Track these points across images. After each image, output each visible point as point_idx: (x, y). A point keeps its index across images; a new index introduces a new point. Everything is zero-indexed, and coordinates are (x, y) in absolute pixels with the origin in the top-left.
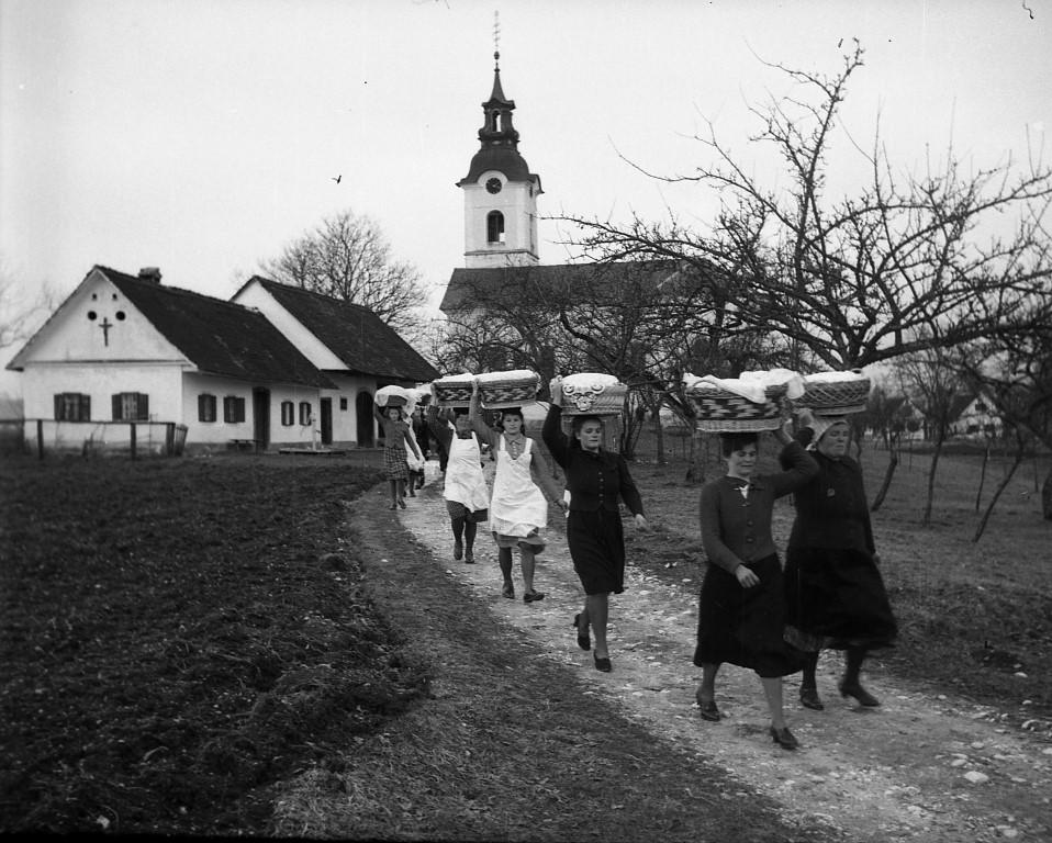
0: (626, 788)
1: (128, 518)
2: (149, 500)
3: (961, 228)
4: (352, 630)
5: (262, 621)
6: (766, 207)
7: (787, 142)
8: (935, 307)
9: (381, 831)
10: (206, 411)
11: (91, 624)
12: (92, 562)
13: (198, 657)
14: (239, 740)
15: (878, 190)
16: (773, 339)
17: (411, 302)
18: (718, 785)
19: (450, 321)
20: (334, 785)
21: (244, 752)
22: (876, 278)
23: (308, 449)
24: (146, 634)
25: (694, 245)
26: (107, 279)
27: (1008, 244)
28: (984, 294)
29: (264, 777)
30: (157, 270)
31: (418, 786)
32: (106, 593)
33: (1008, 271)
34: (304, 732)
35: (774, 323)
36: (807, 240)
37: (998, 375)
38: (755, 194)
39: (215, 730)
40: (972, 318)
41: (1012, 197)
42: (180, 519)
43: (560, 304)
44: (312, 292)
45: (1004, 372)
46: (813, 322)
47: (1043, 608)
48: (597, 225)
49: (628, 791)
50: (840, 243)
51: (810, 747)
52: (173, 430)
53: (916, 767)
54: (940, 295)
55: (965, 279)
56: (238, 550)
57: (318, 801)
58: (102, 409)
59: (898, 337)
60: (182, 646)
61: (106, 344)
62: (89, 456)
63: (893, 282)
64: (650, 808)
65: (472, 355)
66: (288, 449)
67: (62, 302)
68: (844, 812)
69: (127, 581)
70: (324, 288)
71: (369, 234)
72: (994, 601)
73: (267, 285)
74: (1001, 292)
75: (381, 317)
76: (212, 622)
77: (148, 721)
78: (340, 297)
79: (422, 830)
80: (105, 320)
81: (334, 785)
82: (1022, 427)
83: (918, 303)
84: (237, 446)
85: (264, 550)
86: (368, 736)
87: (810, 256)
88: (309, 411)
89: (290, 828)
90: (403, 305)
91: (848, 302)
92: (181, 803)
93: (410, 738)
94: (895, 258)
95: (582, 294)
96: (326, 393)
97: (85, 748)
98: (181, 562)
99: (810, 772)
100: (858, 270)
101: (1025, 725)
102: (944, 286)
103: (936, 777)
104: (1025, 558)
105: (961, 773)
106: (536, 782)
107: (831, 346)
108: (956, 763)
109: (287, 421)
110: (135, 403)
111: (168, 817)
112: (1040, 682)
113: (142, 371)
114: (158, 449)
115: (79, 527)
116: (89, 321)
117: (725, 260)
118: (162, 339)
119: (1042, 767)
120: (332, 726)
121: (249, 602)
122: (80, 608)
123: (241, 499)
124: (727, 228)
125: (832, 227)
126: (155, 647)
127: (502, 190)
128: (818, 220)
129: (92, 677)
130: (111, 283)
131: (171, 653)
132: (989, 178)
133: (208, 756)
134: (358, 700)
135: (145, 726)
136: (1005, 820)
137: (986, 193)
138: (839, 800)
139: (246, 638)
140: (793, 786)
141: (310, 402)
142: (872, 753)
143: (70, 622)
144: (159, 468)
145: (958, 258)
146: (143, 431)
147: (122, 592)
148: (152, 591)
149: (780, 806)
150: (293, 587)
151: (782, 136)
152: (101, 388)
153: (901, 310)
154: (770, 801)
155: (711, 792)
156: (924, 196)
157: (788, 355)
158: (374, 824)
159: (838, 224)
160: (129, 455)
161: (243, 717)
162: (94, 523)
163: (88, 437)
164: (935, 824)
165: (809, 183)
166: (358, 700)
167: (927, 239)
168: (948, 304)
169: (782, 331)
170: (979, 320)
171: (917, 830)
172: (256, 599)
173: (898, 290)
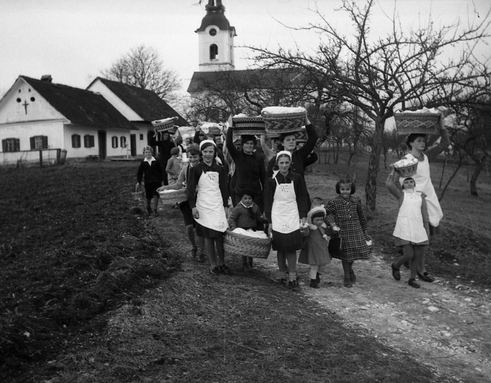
0: (272, 310)
1: (39, 195)
2: (49, 186)
3: (435, 54)
4: (145, 241)
5: (102, 239)
6: (342, 42)
7: (352, 11)
8: (421, 91)
9: (158, 331)
10: (76, 142)
11: (21, 245)
12: (21, 216)
13: (71, 256)
14: (91, 293)
15: (395, 35)
16: (345, 106)
17: (174, 88)
18: (314, 309)
19: (192, 97)
20: (136, 311)
21: (93, 298)
22: (393, 76)
23: (125, 159)
24: (48, 248)
25: (307, 60)
26: (25, 82)
27: (456, 62)
28: (444, 85)
29: (102, 310)
30: (50, 76)
31: (175, 311)
32: (28, 230)
33: (456, 75)
34: (122, 288)
35: (345, 97)
36: (361, 58)
37: (451, 125)
38: (336, 36)
39: (80, 289)
40: (438, 97)
41: (459, 40)
42: (64, 194)
43: (245, 88)
44: (126, 84)
45: (454, 124)
46: (363, 97)
47: (468, 235)
48: (261, 50)
49: (273, 312)
50: (376, 60)
51: (358, 293)
52: (60, 152)
53: (406, 303)
54: (423, 85)
55: (436, 78)
56: (91, 206)
57: (128, 319)
58: (25, 145)
59: (403, 105)
60: (64, 252)
61: (26, 113)
62: (20, 168)
63: (401, 78)
64: (283, 319)
65: (203, 113)
66: (115, 159)
67: (4, 94)
68: (372, 322)
69: (39, 224)
70: (131, 82)
71: (153, 55)
72: (445, 230)
73: (104, 81)
74: (453, 85)
75: (159, 96)
76: (79, 240)
77: (47, 287)
78: (139, 86)
79: (177, 330)
80: (25, 102)
81: (136, 311)
82: (462, 151)
83: (413, 89)
84: (91, 158)
85: (103, 206)
86: (152, 289)
87: (363, 66)
88: (125, 141)
89: (115, 331)
90: (169, 90)
91: (380, 88)
92: (64, 323)
93: (171, 289)
94: (402, 67)
95: (255, 84)
96: (133, 132)
97: (18, 302)
98: (64, 214)
99: (357, 304)
100: (384, 73)
101: (457, 287)
102: (426, 80)
103: (415, 308)
104: (461, 211)
105: (426, 307)
106: (230, 308)
107: (371, 109)
108: (424, 302)
109: (115, 145)
110: (41, 141)
111: (58, 329)
112: (465, 268)
113: (44, 125)
114: (53, 162)
115: (15, 201)
116: (18, 103)
117: (322, 67)
118: (53, 109)
119: (464, 306)
120: (135, 284)
121: (96, 230)
122: (15, 238)
123: (93, 183)
124: (323, 52)
125: (372, 52)
126: (52, 253)
127: (217, 34)
128: (366, 49)
129: (21, 269)
130: (28, 84)
131: (58, 255)
132: (448, 31)
133: (76, 301)
134: (147, 273)
135: (46, 290)
136: (445, 329)
137: (447, 37)
138: (370, 317)
139: (94, 246)
140: (349, 310)
141: (125, 136)
142: (386, 296)
143: (11, 245)
144: (53, 170)
145: (432, 68)
146: (45, 154)
147: (36, 229)
148: (50, 228)
149: (343, 319)
150: (117, 222)
151: (350, 8)
152: (24, 134)
153: (405, 92)
154: (338, 317)
155: (311, 312)
156: (417, 38)
157: (352, 113)
158: (154, 328)
159: (375, 51)
160: (39, 165)
161: (92, 283)
162: (23, 198)
163: (19, 158)
164: (413, 329)
165: (362, 29)
166: (147, 273)
167: (417, 58)
168: (427, 90)
169: (349, 101)
170: (442, 98)
171: (405, 331)
172: (99, 228)
173: (404, 82)
